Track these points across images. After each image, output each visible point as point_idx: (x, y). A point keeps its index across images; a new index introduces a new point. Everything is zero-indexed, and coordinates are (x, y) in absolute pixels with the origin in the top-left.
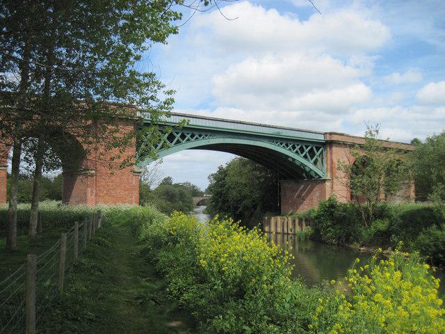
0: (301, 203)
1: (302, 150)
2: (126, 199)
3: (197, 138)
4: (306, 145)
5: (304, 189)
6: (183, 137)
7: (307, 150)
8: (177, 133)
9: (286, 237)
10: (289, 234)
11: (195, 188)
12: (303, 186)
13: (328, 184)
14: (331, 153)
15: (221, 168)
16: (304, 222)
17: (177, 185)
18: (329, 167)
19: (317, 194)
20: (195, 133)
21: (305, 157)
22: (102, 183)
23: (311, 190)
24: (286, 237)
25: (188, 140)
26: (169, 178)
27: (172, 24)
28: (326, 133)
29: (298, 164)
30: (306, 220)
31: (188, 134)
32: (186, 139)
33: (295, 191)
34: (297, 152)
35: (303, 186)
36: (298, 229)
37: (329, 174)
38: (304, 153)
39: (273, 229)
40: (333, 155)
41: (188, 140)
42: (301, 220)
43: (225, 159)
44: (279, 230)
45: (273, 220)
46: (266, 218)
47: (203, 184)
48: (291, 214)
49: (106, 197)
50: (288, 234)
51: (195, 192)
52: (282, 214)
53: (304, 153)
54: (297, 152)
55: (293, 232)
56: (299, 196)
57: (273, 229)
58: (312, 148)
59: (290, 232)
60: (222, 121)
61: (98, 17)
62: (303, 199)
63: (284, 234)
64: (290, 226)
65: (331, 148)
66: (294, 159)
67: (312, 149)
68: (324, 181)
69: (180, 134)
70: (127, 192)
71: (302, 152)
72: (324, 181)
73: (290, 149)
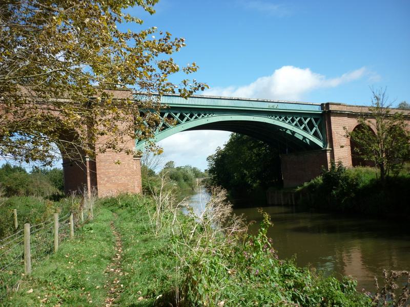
3: (196, 118)
4: (305, 117)
6: (182, 117)
7: (306, 122)
15: (361, 257)
17: (179, 169)
21: (305, 129)
22: (102, 171)
25: (188, 120)
26: (172, 162)
27: (4, 193)
29: (301, 138)
31: (187, 114)
32: (186, 119)
34: (296, 125)
43: (223, 138)
47: (203, 166)
51: (197, 174)
53: (303, 126)
54: (296, 125)
58: (310, 120)
60: (227, 106)
66: (294, 133)
67: (300, 120)
70: (128, 178)
71: (293, 122)
73: (289, 122)
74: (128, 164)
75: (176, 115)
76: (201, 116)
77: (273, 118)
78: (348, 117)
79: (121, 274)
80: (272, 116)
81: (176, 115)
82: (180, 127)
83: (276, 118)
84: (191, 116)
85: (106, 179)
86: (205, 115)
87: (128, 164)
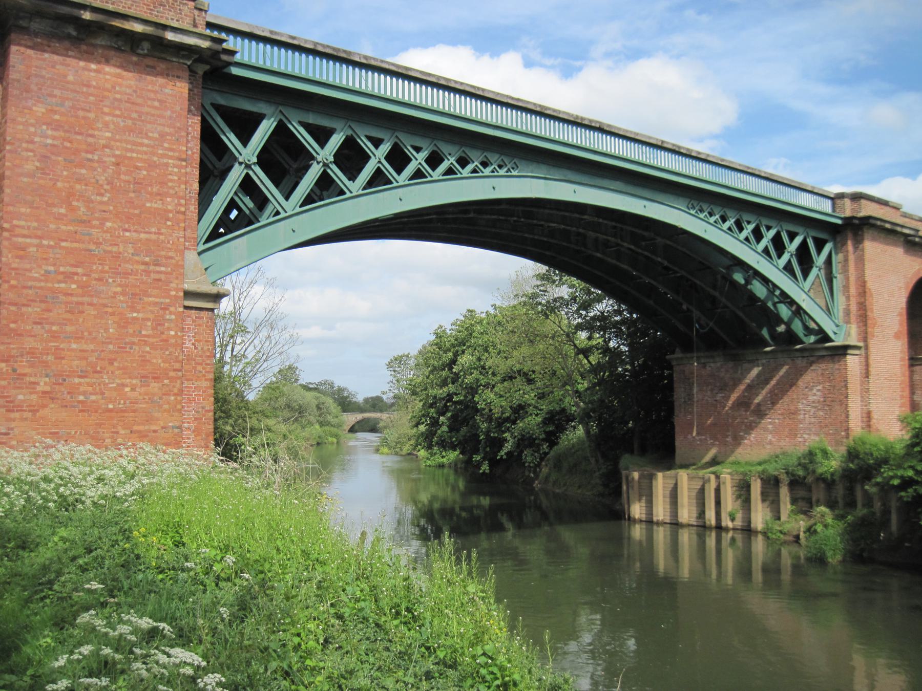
0: (750, 427)
1: (779, 245)
2: (149, 420)
3: (450, 171)
4: (792, 228)
5: (762, 380)
6: (398, 159)
8: (377, 143)
9: (711, 541)
10: (727, 530)
11: (345, 394)
12: (755, 371)
13: (853, 361)
14: (860, 261)
16: (784, 492)
18: (854, 308)
19: (816, 395)
20: (445, 148)
22: (29, 343)
23: (789, 383)
24: (711, 541)
25: (418, 174)
28: (841, 196)
30: (795, 483)
31: (418, 149)
33: (726, 387)
35: (755, 371)
36: (760, 517)
37: (854, 329)
38: (786, 257)
39: (661, 512)
40: (868, 266)
41: (418, 174)
42: (771, 484)
44: (686, 514)
45: (661, 482)
46: (636, 475)
48: (714, 462)
49: (51, 412)
50: (719, 528)
52: (678, 458)
54: (766, 251)
55: (738, 523)
56: (743, 403)
57: (661, 512)
59: (726, 522)
60: (601, 129)
61: (203, 318)
62: (760, 413)
63: (703, 527)
64: (730, 502)
65: (858, 241)
68: (843, 351)
69: (385, 148)
70: (154, 386)
72: (843, 351)
74: (159, 323)
75: (377, 147)
76: (470, 167)
77: (702, 216)
78: (907, 252)
79: (150, 188)
80: (701, 211)
81: (377, 147)
82: (282, 232)
83: (712, 220)
84: (434, 160)
85: (43, 385)
86: (485, 164)
87: (159, 323)
